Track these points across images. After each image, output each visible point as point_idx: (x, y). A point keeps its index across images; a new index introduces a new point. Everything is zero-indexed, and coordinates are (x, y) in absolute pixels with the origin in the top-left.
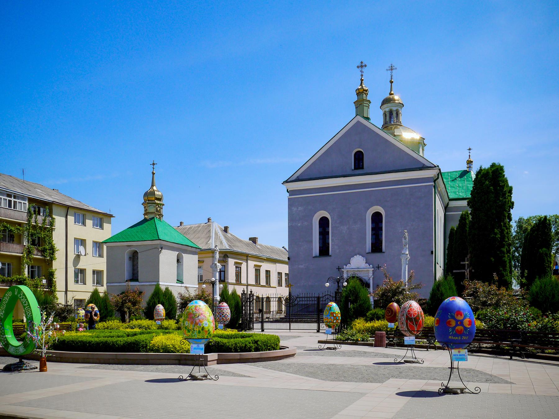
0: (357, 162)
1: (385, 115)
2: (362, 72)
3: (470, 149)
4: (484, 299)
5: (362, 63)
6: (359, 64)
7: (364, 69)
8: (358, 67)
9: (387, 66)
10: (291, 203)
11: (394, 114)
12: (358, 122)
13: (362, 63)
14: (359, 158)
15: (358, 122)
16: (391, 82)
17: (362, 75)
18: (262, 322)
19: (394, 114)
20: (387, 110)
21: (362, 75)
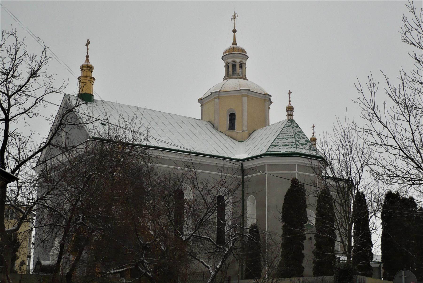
16: (234, 31)
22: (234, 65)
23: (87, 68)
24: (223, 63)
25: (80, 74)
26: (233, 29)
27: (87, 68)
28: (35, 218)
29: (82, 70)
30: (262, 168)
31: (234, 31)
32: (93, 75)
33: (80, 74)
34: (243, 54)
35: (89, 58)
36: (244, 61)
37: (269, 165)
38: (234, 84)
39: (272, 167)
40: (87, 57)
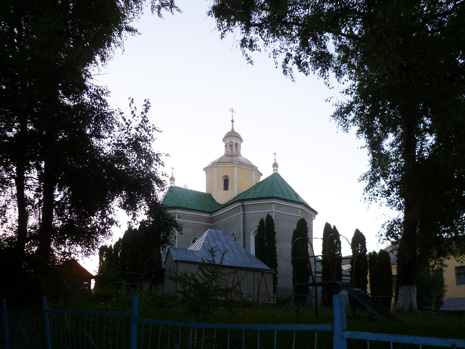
1: (226, 146)
11: (234, 146)
16: (233, 121)
19: (234, 146)
20: (228, 142)
24: (224, 144)
31: (233, 121)
34: (237, 136)
36: (239, 143)
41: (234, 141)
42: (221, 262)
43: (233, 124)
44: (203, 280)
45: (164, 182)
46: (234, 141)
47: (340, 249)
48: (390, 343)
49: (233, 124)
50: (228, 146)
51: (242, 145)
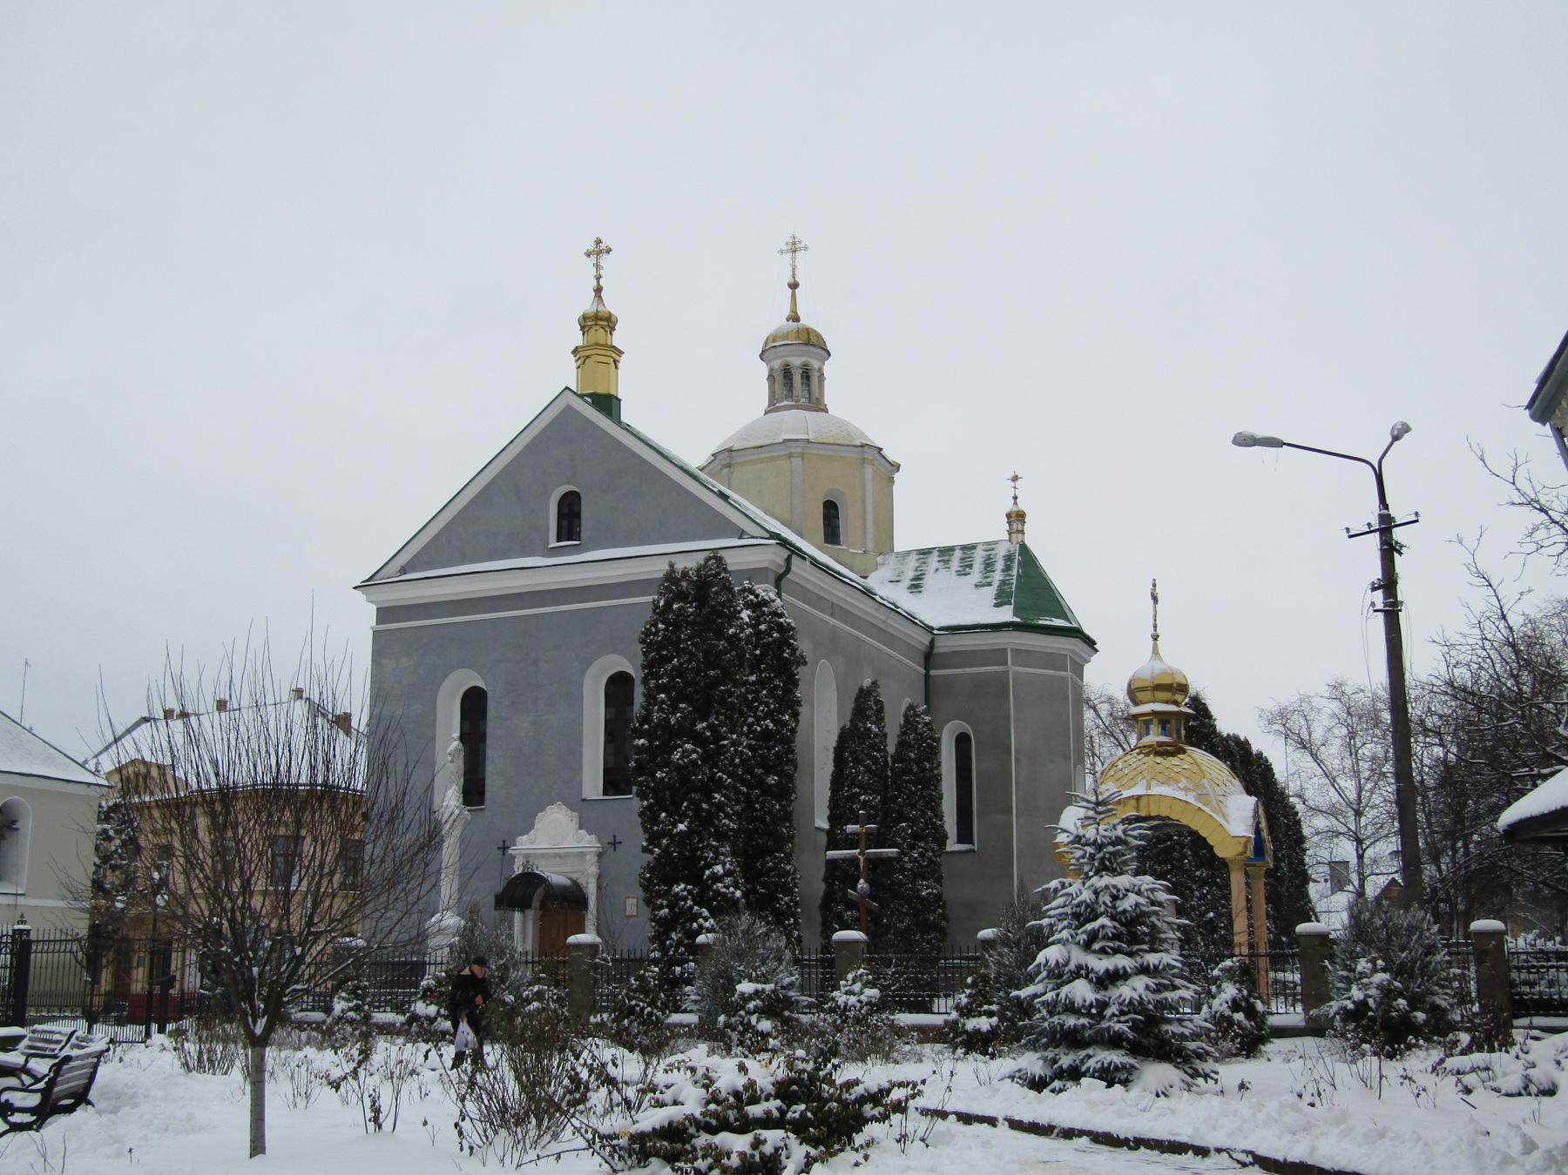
0: (565, 523)
1: (771, 378)
2: (597, 266)
3: (1015, 479)
4: (156, 813)
5: (598, 242)
6: (591, 246)
7: (605, 260)
8: (588, 254)
9: (783, 241)
10: (382, 644)
11: (797, 378)
12: (568, 407)
13: (598, 242)
14: (570, 511)
15: (568, 407)
16: (794, 286)
17: (598, 278)
18: (365, 1037)
19: (797, 378)
20: (777, 364)
21: (598, 278)
22: (787, 373)
23: (598, 322)
24: (763, 370)
25: (578, 339)
26: (789, 279)
27: (598, 322)
28: (689, 902)
29: (582, 328)
30: (998, 656)
31: (794, 286)
32: (617, 339)
33: (578, 339)
34: (812, 341)
35: (603, 294)
36: (815, 364)
37: (1017, 652)
38: (795, 423)
39: (1023, 656)
40: (598, 290)
41: (796, 361)
42: (256, 1077)
43: (794, 296)
44: (139, 751)
45: (1380, 606)
46: (796, 361)
47: (104, 1022)
48: (832, 863)
49: (794, 296)
50: (779, 378)
51: (828, 368)
